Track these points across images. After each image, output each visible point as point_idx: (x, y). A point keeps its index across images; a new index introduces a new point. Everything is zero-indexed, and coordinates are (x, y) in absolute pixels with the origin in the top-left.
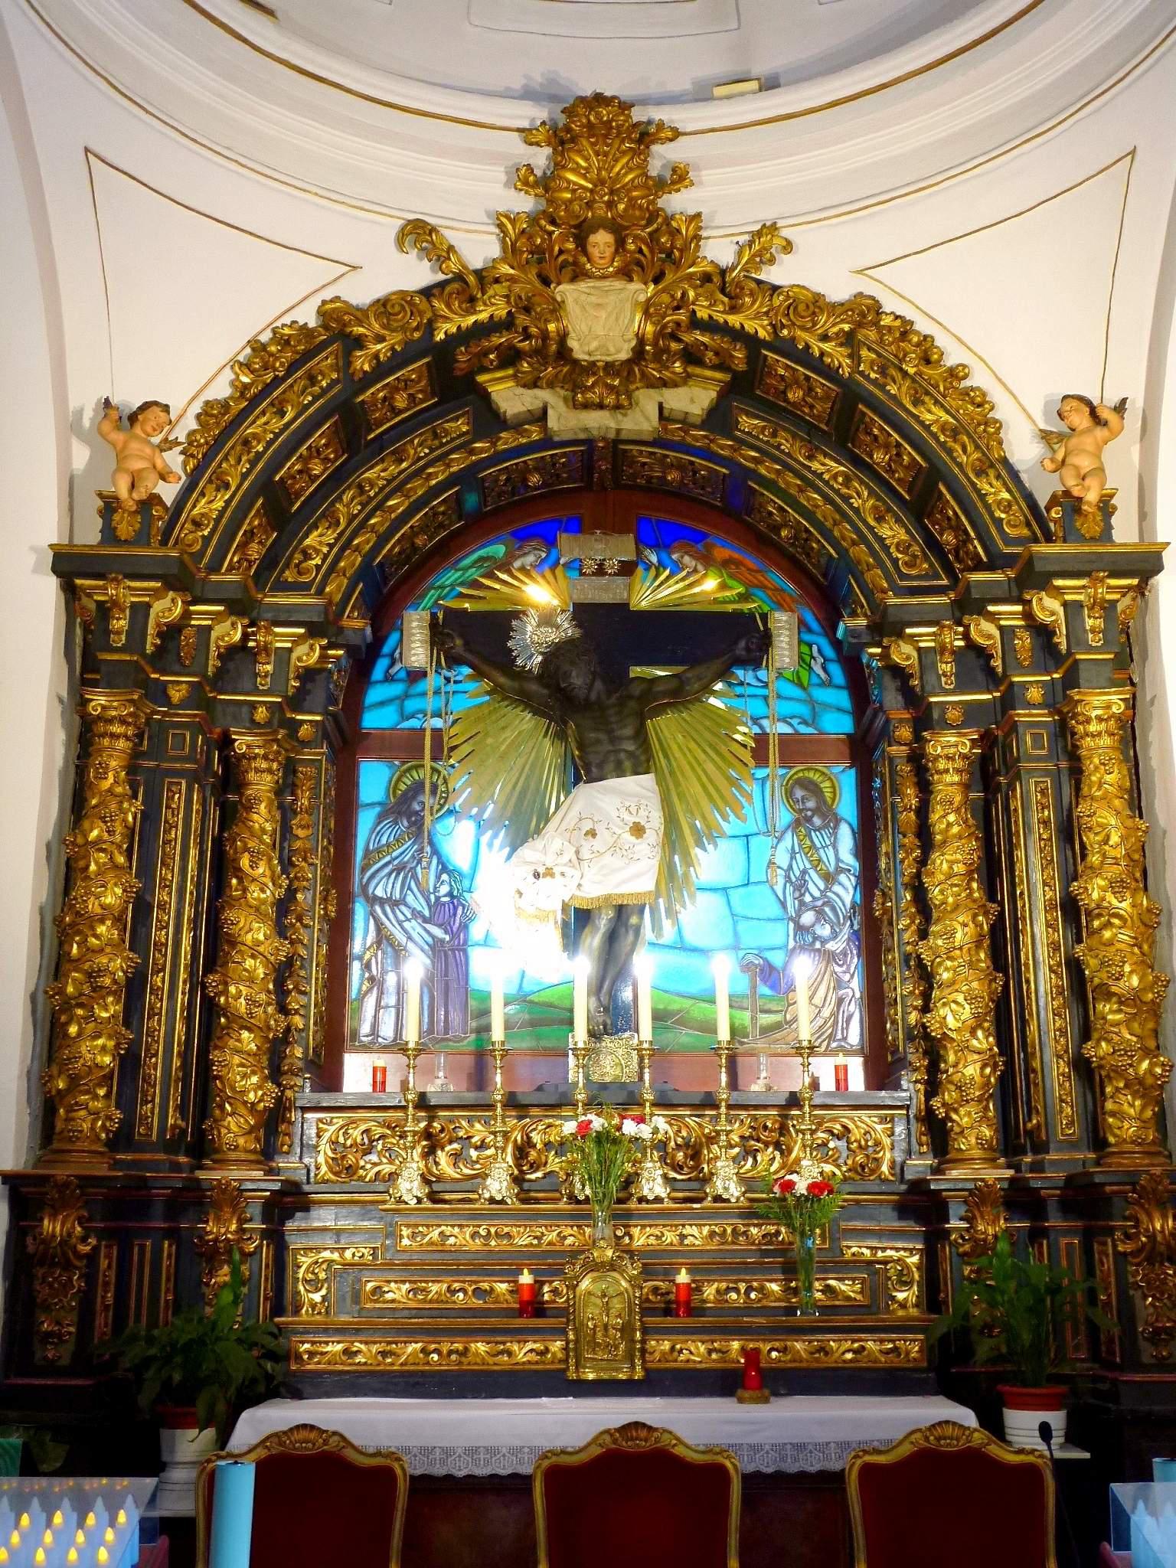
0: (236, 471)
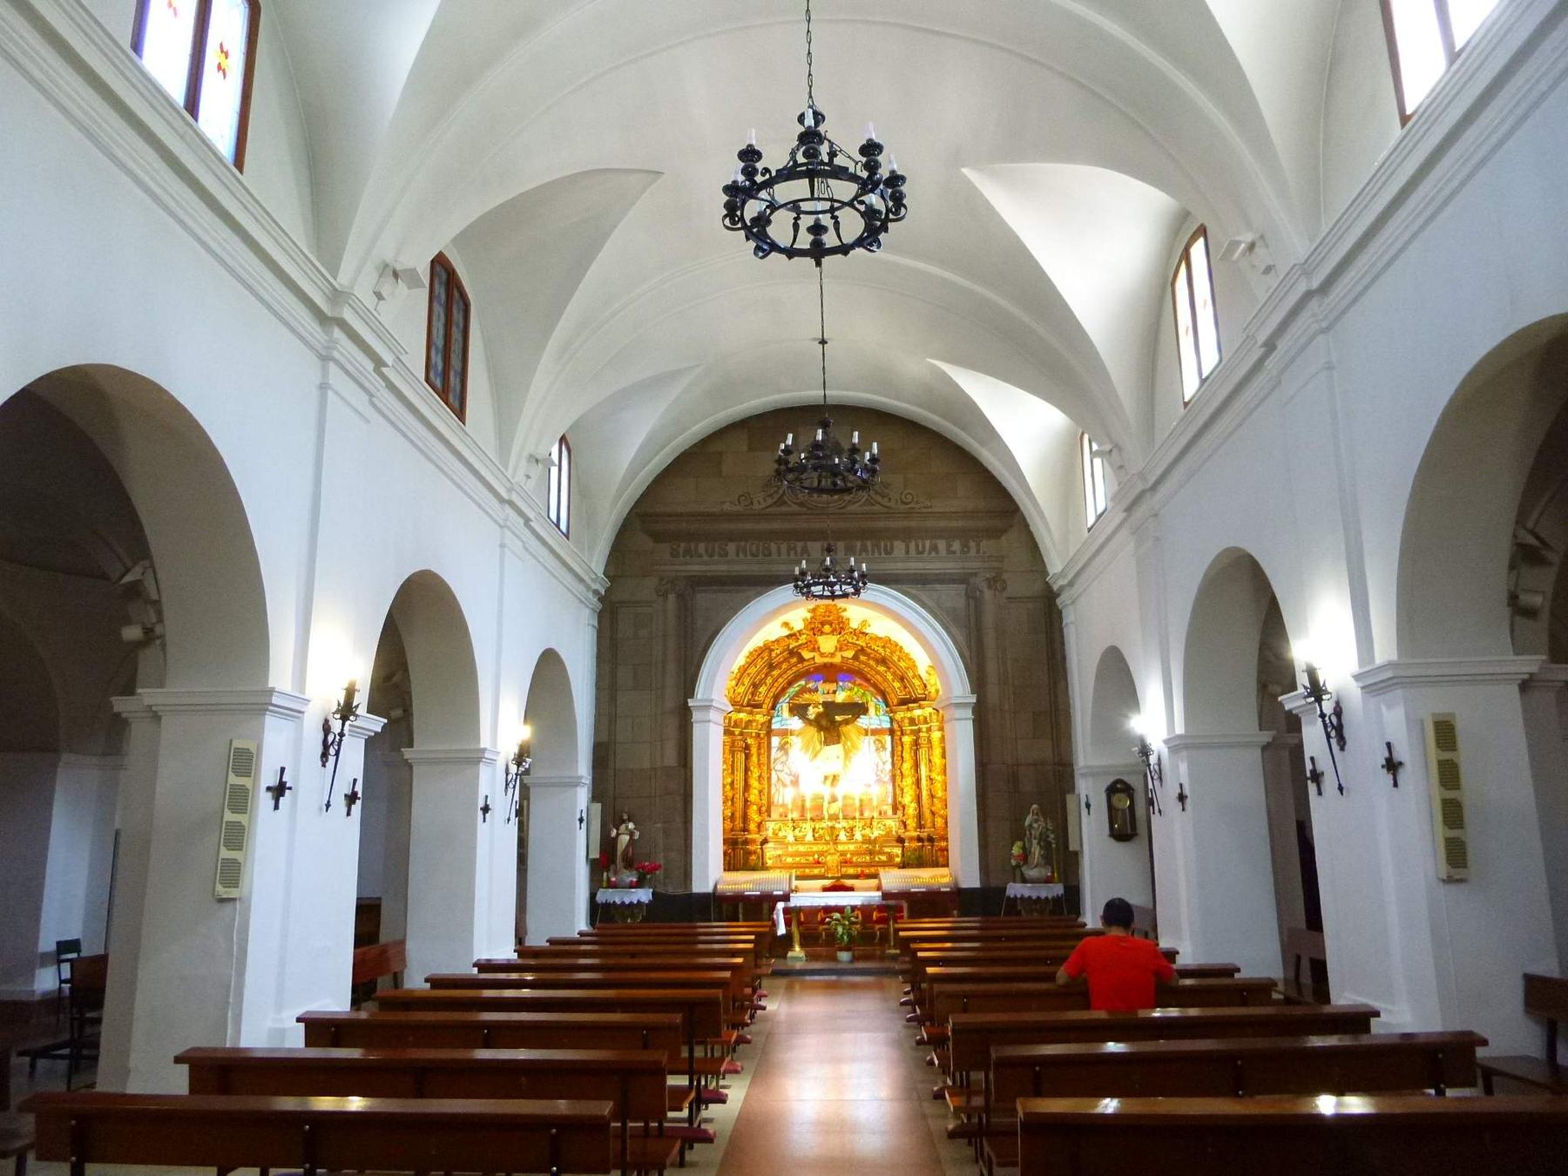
0: (746, 681)
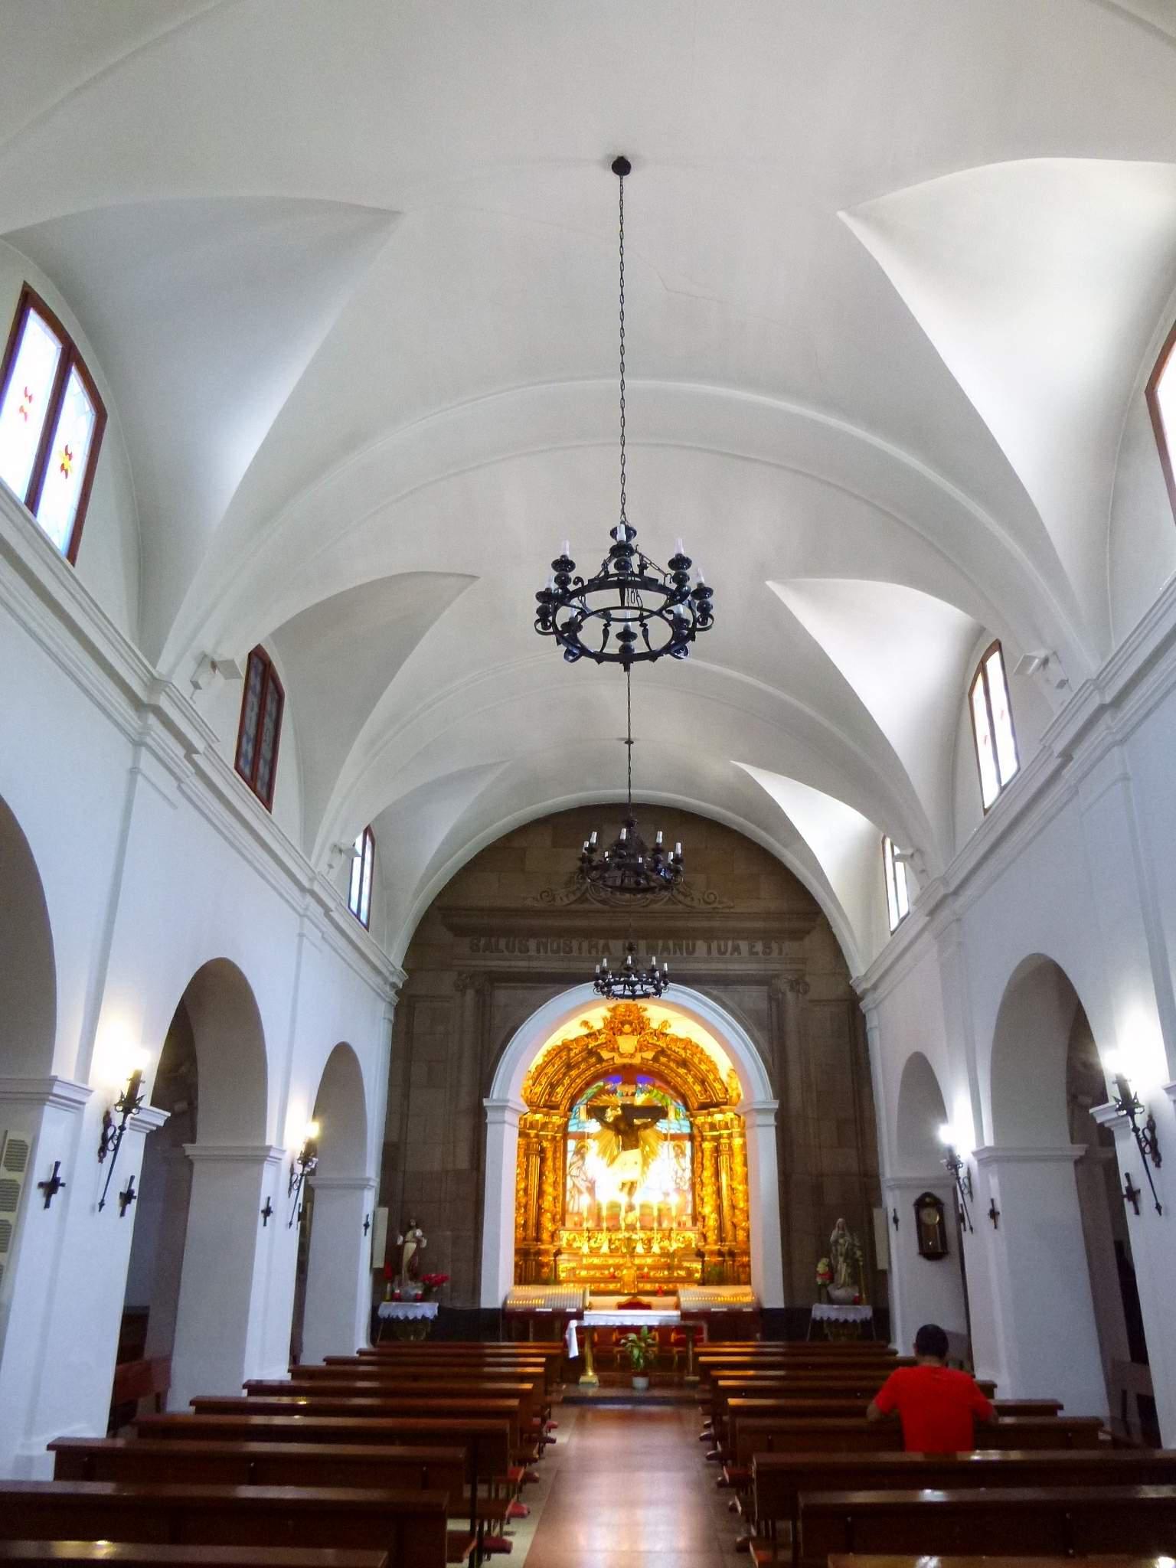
0: (544, 1081)
